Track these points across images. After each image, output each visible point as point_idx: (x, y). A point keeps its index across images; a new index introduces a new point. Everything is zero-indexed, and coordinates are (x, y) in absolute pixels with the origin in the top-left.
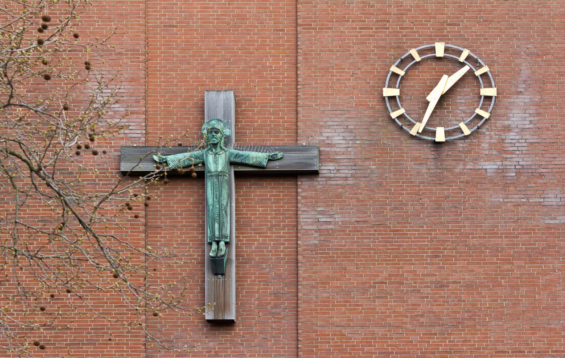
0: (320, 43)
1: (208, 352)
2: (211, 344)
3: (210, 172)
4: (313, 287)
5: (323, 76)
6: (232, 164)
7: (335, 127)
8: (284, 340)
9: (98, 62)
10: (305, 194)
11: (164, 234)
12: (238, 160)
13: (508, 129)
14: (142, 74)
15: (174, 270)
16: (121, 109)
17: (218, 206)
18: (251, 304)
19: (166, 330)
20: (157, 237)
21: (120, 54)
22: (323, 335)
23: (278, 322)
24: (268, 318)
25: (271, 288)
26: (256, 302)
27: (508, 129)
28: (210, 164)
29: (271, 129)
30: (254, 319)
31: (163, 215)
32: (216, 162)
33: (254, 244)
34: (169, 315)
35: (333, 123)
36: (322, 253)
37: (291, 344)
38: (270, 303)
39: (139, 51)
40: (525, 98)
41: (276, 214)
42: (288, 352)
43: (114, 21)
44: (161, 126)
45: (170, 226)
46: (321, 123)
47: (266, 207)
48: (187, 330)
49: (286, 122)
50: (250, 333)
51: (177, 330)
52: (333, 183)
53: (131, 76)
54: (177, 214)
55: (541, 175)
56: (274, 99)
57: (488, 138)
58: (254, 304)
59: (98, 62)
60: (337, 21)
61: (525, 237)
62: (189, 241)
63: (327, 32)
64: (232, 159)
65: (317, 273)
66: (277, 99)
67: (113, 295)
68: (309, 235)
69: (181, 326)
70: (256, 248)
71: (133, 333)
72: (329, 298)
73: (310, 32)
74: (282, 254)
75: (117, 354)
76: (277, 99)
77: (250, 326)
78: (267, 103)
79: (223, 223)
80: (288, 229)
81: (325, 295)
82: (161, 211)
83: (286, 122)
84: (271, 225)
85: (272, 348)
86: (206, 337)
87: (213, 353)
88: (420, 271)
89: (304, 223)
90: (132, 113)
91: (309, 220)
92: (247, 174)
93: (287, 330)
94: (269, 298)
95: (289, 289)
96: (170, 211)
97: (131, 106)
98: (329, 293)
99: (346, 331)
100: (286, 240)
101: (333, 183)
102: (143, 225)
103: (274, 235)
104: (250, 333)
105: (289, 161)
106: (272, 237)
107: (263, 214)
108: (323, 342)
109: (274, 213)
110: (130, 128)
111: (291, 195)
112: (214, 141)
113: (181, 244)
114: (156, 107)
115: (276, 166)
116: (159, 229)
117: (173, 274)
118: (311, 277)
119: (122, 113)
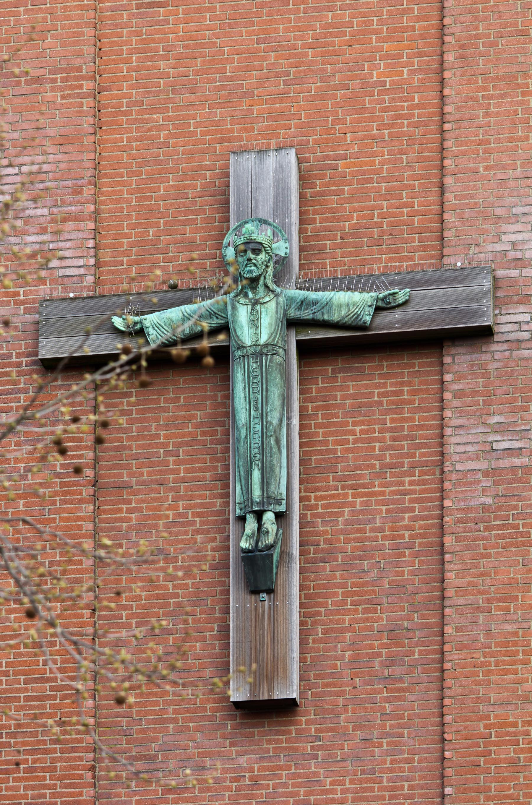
1: (236, 779)
2: (243, 761)
4: (480, 610)
5: (503, 96)
6: (292, 324)
8: (411, 742)
12: (306, 314)
15: (159, 587)
17: (259, 427)
18: (336, 658)
19: (139, 732)
21: (38, 80)
22: (503, 725)
24: (375, 692)
25: (380, 619)
26: (347, 653)
28: (242, 328)
29: (383, 233)
30: (342, 694)
32: (255, 323)
33: (342, 514)
38: (379, 655)
39: (80, 69)
42: (420, 770)
44: (131, 245)
45: (151, 482)
47: (370, 422)
50: (332, 730)
51: (165, 730)
53: (63, 131)
58: (343, 657)
62: (194, 515)
65: (489, 574)
66: (395, 161)
68: (471, 483)
69: (175, 720)
70: (346, 522)
72: (516, 634)
74: (407, 534)
75: (30, 793)
77: (332, 711)
78: (373, 172)
80: (422, 473)
81: (508, 627)
83: (417, 213)
86: (232, 745)
87: (247, 782)
89: (457, 457)
91: (470, 448)
93: (419, 716)
94: (376, 643)
95: (423, 617)
96: (150, 446)
97: (64, 203)
98: (515, 621)
102: (89, 483)
103: (388, 490)
104: (332, 730)
106: (383, 493)
108: (503, 743)
109: (387, 435)
110: (61, 253)
112: (251, 272)
114: (118, 201)
117: (158, 597)
119: (42, 220)
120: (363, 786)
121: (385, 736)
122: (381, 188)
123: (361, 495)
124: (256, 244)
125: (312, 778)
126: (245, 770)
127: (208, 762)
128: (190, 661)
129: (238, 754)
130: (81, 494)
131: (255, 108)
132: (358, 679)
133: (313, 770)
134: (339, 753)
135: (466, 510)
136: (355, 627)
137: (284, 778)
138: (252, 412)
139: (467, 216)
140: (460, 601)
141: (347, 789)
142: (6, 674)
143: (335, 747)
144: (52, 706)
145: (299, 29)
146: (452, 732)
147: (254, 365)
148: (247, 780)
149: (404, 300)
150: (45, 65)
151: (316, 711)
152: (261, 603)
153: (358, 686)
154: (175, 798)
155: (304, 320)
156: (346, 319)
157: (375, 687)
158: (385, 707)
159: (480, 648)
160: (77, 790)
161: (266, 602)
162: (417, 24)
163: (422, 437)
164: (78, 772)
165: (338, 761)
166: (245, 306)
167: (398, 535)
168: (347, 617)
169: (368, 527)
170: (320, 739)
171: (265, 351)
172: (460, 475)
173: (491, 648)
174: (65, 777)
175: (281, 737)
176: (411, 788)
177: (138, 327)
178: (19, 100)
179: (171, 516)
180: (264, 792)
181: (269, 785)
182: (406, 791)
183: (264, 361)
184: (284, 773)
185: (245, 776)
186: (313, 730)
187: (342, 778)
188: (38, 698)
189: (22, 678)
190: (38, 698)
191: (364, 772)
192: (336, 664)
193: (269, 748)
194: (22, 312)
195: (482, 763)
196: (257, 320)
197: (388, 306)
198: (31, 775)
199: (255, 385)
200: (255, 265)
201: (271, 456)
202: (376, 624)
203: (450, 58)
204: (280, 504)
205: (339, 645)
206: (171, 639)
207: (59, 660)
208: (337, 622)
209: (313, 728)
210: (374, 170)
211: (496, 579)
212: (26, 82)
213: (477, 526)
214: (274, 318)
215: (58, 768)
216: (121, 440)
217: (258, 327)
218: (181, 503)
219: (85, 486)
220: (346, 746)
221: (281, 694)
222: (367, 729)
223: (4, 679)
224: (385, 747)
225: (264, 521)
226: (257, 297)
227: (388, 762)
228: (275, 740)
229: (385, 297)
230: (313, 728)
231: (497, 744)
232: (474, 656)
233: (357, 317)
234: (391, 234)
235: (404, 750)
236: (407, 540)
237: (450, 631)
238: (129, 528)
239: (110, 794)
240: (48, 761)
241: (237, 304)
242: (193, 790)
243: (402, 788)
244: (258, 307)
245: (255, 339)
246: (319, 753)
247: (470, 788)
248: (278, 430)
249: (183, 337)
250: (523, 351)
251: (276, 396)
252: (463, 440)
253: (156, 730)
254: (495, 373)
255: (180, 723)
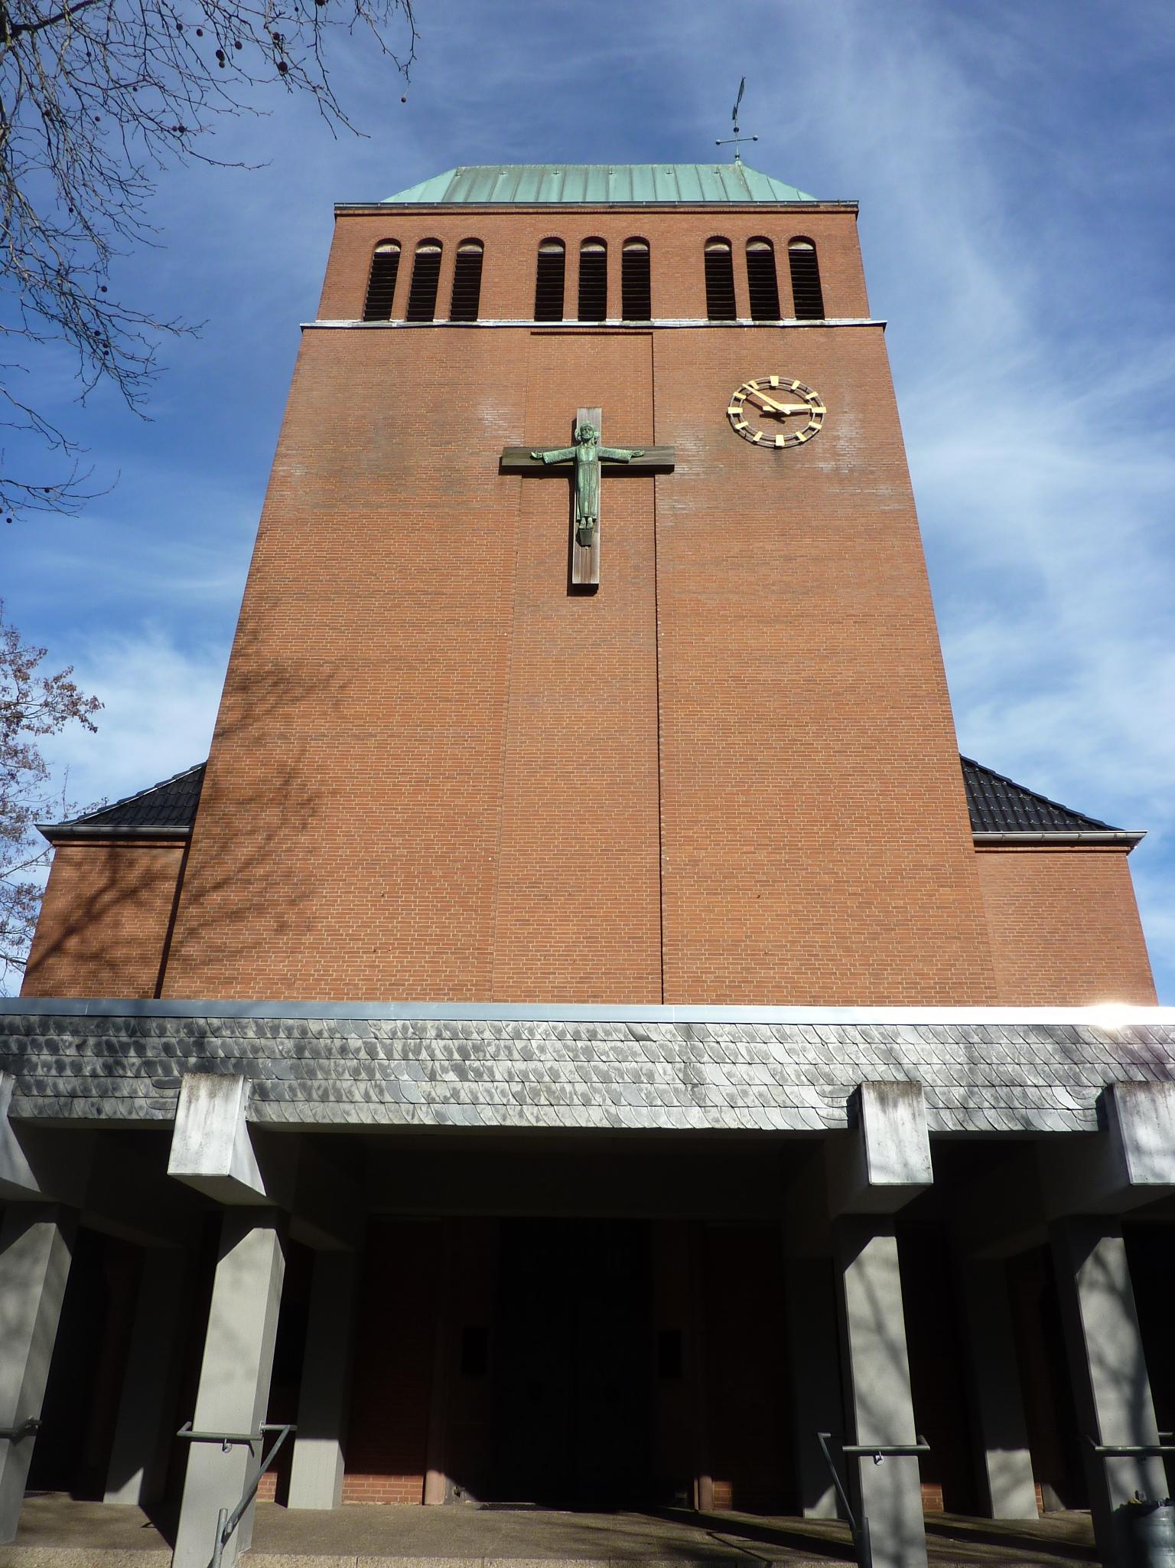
6: (601, 459)
13: (838, 438)
27: (838, 438)
32: (587, 454)
40: (846, 417)
55: (872, 472)
57: (820, 446)
61: (863, 520)
88: (769, 547)
92: (613, 469)
99: (702, 597)
115: (638, 461)
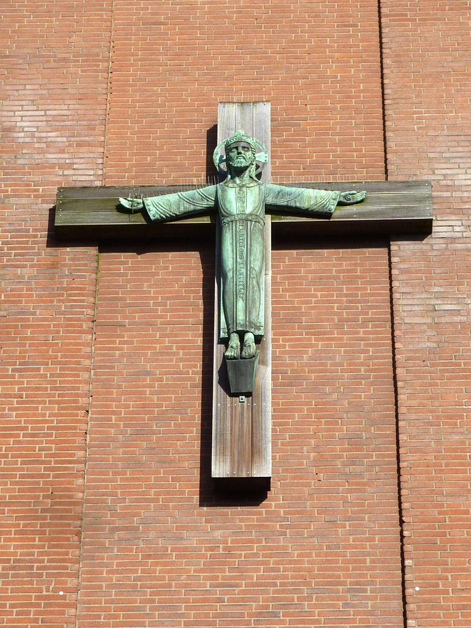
0: (423, 39)
1: (211, 549)
2: (218, 534)
3: (231, 215)
4: (431, 424)
5: (431, 86)
6: (271, 209)
7: (459, 160)
8: (372, 525)
9: (24, 72)
10: (406, 266)
11: (129, 337)
12: (282, 202)
14: (101, 88)
15: (145, 399)
16: (59, 139)
17: (244, 271)
18: (302, 457)
19: (122, 508)
20: (114, 342)
21: (64, 60)
22: (455, 512)
23: (359, 491)
24: (338, 484)
25: (341, 430)
26: (312, 455)
28: (230, 202)
29: (338, 167)
30: (309, 485)
31: (129, 305)
32: (242, 199)
33: (306, 352)
34: (132, 479)
35: (455, 155)
36: (444, 365)
37: (388, 532)
38: (341, 457)
39: (98, 55)
41: (350, 302)
42: (381, 547)
43: (57, 16)
44: (132, 166)
45: (141, 324)
46: (431, 155)
47: (329, 290)
48: (167, 507)
49: (364, 156)
50: (299, 512)
51: (147, 508)
52: (460, 246)
53: (81, 91)
54: (155, 304)
56: (341, 123)
58: (308, 457)
59: (24, 72)
60: (451, 9)
62: (178, 348)
63: (434, 25)
64: (270, 200)
65: (437, 398)
66: (345, 123)
67: (19, 442)
68: (417, 333)
69: (156, 500)
70: (310, 358)
71: (57, 511)
72: (463, 443)
73: (404, 25)
74: (363, 368)
75: (19, 551)
76: (345, 123)
77: (299, 498)
78: (329, 129)
79: (254, 300)
80: (374, 326)
81: (456, 437)
82: (124, 299)
83: (364, 156)
84: (339, 321)
85: (348, 540)
86: (207, 521)
87: (221, 551)
89: (405, 314)
90: (79, 145)
91: (416, 308)
92: (298, 231)
93: (378, 505)
94: (338, 447)
95: (379, 429)
96: (142, 298)
97: (79, 135)
98: (462, 433)
100: (371, 345)
101: (460, 246)
102: (88, 320)
103: (345, 337)
104: (299, 512)
105: (378, 207)
106: (342, 339)
107: (323, 302)
108: (457, 527)
109: (345, 299)
110: (75, 166)
111: (377, 271)
112: (241, 163)
113: (161, 354)
114: (123, 138)
116: (118, 328)
117: (144, 406)
118: (424, 405)
119: (61, 145)
120: (328, 558)
121: (348, 519)
122: (335, 139)
123: (323, 340)
124: (245, 143)
125: (281, 550)
126: (219, 542)
127: (185, 534)
128: (171, 455)
129: (212, 529)
130: (81, 327)
131: (234, 87)
132: (322, 475)
133: (282, 544)
134: (306, 532)
135: (415, 351)
136: (319, 435)
137: (256, 549)
138: (238, 260)
139: (406, 156)
140: (413, 416)
141: (314, 560)
142: (6, 456)
143: (302, 526)
144: (45, 483)
145: (269, 42)
146: (410, 516)
147: (241, 227)
148: (221, 550)
149: (361, 198)
150: (70, 51)
151: (285, 498)
152: (240, 403)
153: (322, 480)
154: (154, 562)
155: (280, 206)
156: (315, 207)
157: (338, 480)
158: (347, 496)
159: (432, 452)
160: (64, 550)
161: (245, 403)
162: (361, 44)
163: (373, 301)
164: (65, 536)
165: (304, 538)
166: (234, 189)
167: (355, 369)
168: (312, 427)
169: (329, 362)
170: (288, 519)
171: (250, 218)
172: (409, 326)
173: (442, 452)
174: (53, 539)
175: (252, 517)
176: (372, 561)
177: (141, 206)
178: (49, 71)
179: (158, 348)
180: (237, 560)
181: (241, 554)
182: (368, 564)
183: (249, 225)
184: (255, 545)
185: (219, 547)
186: (282, 512)
187: (309, 551)
188: (32, 476)
189: (19, 460)
190: (32, 476)
191: (328, 547)
192: (303, 462)
193: (242, 525)
194: (40, 202)
195: (439, 542)
196: (244, 197)
197: (348, 202)
198: (21, 536)
199: (241, 241)
200: (244, 158)
201: (253, 292)
202: (337, 433)
203: (388, 62)
204: (259, 330)
205: (305, 448)
206: (155, 438)
207: (54, 447)
208: (302, 430)
209: (282, 511)
210: (330, 128)
211: (443, 402)
212: (54, 61)
213: (425, 363)
214: (257, 198)
215: (47, 532)
216: (117, 293)
217: (244, 202)
218: (167, 339)
219: (86, 321)
220: (312, 526)
221: (257, 473)
222: (331, 513)
223: (3, 460)
224: (348, 528)
225: (245, 339)
226: (244, 183)
227: (351, 540)
228: (247, 519)
229: (346, 195)
230: (282, 511)
231: (451, 527)
232: (427, 458)
233: (324, 206)
234: (344, 168)
235: (365, 531)
236: (363, 373)
237: (405, 438)
238: (121, 356)
239: (94, 556)
240: (39, 526)
241: (226, 188)
242: (170, 556)
243: (364, 561)
244: (244, 189)
245: (241, 209)
246: (288, 531)
247: (428, 562)
248: (258, 276)
249: (178, 213)
250: (456, 245)
251: (258, 250)
252: (410, 302)
253: (138, 507)
254: (434, 258)
255: (161, 502)
